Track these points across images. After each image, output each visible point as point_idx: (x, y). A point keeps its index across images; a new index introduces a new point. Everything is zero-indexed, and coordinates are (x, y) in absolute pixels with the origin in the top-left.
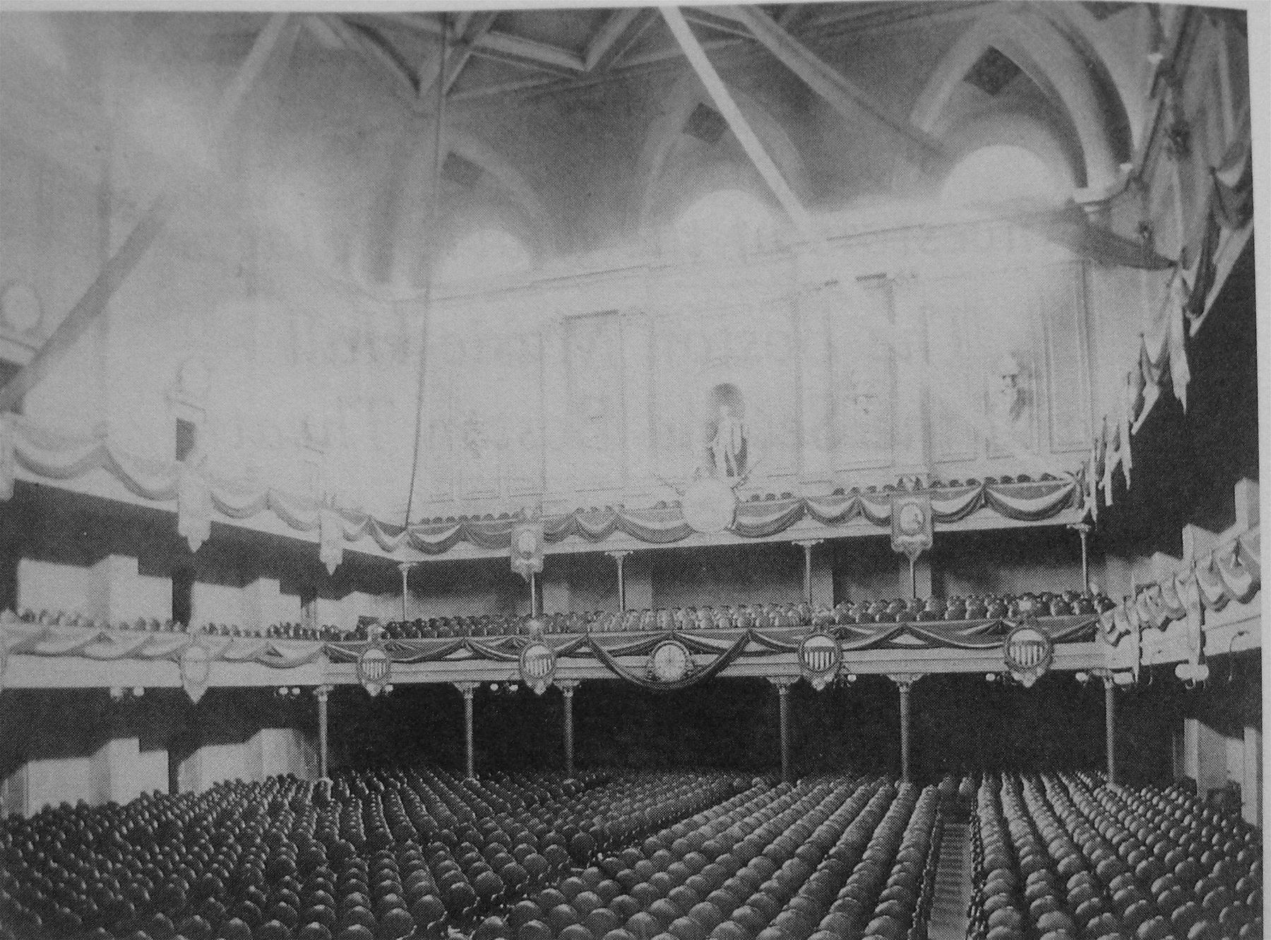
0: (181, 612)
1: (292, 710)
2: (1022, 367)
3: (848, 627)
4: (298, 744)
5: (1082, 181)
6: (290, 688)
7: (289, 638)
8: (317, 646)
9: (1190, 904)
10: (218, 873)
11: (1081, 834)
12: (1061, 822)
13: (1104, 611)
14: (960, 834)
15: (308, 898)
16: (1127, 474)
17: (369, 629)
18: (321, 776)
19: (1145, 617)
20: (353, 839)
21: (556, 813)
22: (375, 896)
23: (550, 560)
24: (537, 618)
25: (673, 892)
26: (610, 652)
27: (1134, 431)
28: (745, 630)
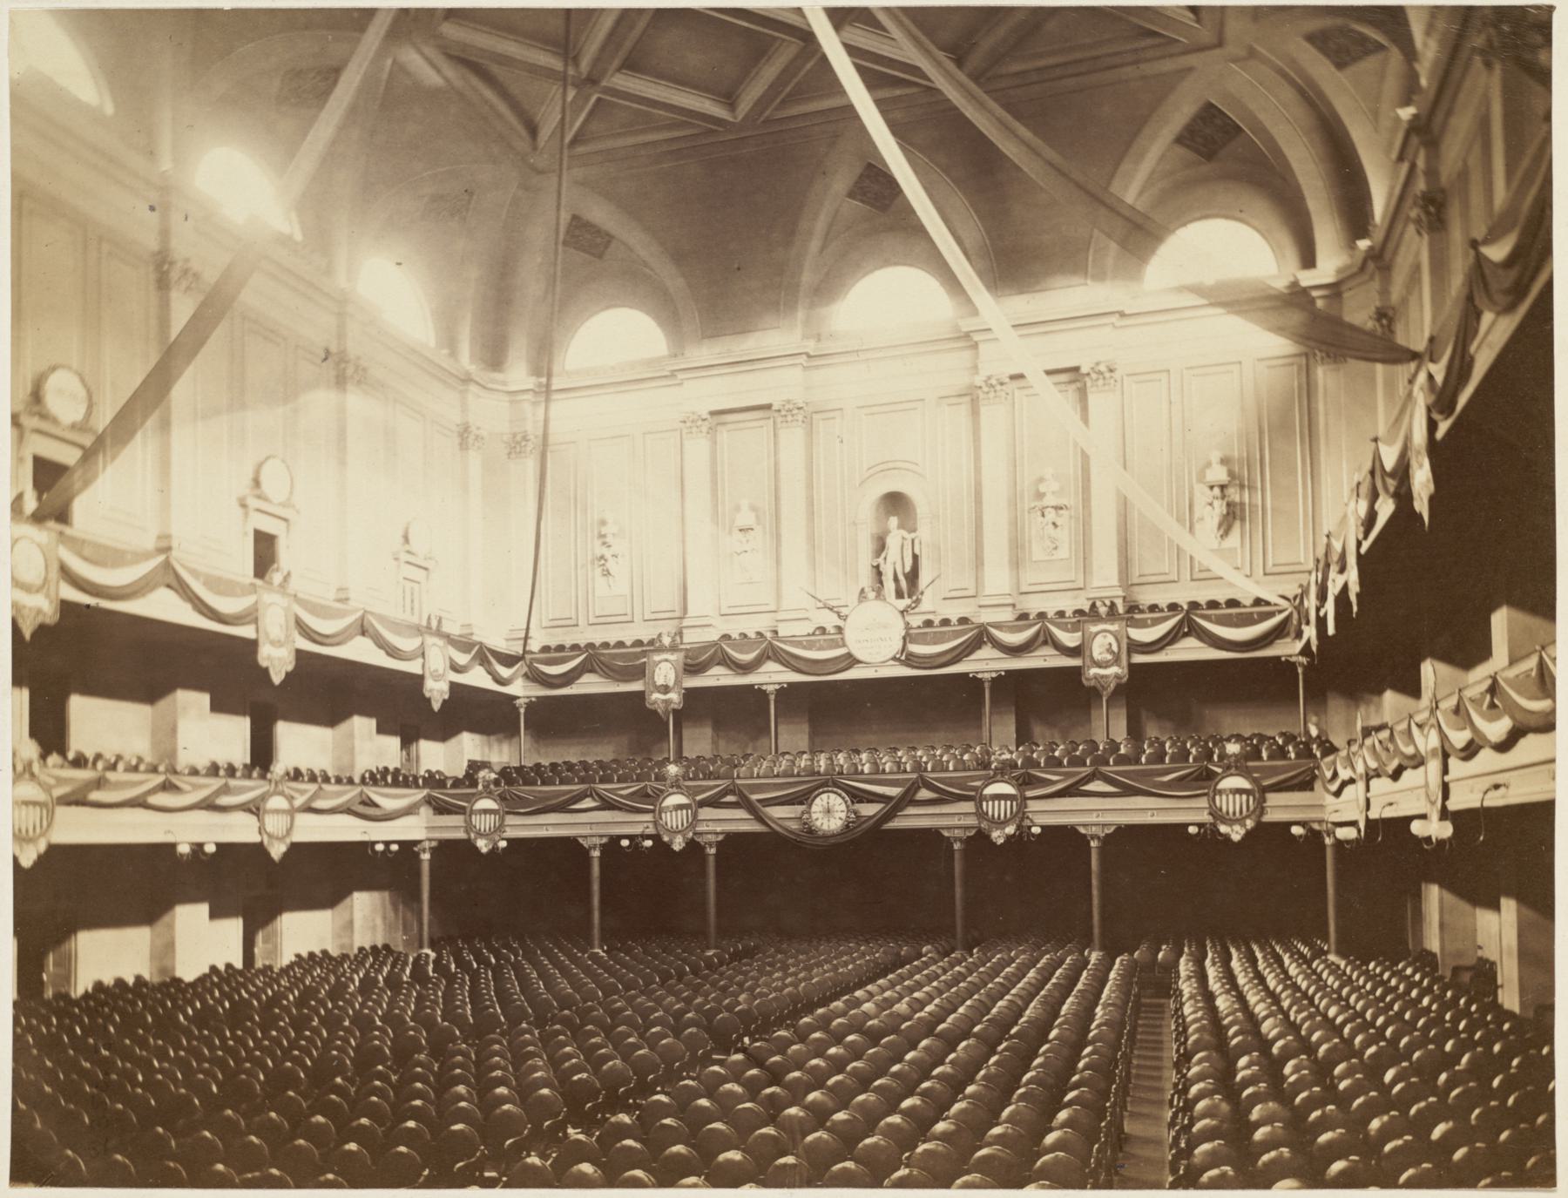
0: (262, 753)
1: (387, 869)
2: (1231, 474)
3: (1032, 772)
4: (396, 910)
5: (1308, 261)
6: (387, 843)
7: (387, 785)
8: (418, 795)
9: (1432, 1099)
10: (298, 1061)
11: (1298, 1012)
12: (1275, 998)
13: (1324, 755)
14: (1161, 1008)
15: (403, 1091)
16: (1353, 598)
17: (482, 774)
18: (421, 947)
19: (1373, 764)
20: (459, 1021)
21: (697, 990)
22: (483, 1088)
23: (691, 695)
24: (675, 762)
25: (831, 1082)
26: (759, 801)
27: (1363, 550)
28: (914, 776)
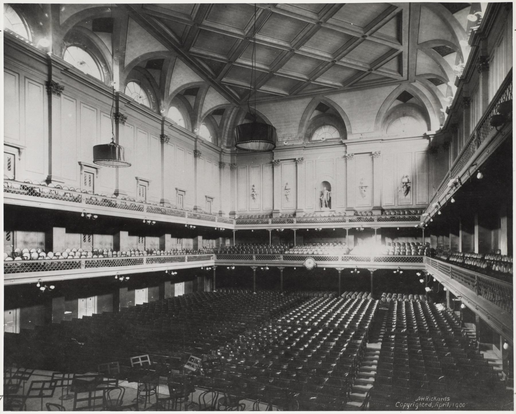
5: (429, 129)
